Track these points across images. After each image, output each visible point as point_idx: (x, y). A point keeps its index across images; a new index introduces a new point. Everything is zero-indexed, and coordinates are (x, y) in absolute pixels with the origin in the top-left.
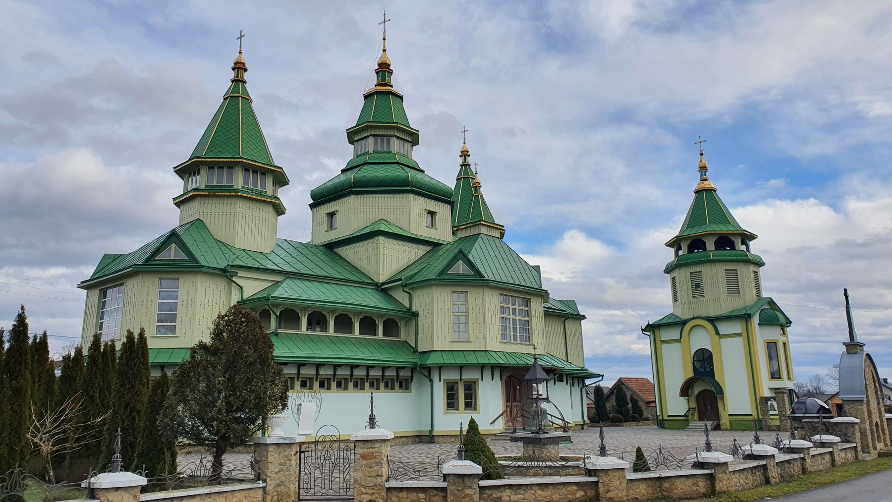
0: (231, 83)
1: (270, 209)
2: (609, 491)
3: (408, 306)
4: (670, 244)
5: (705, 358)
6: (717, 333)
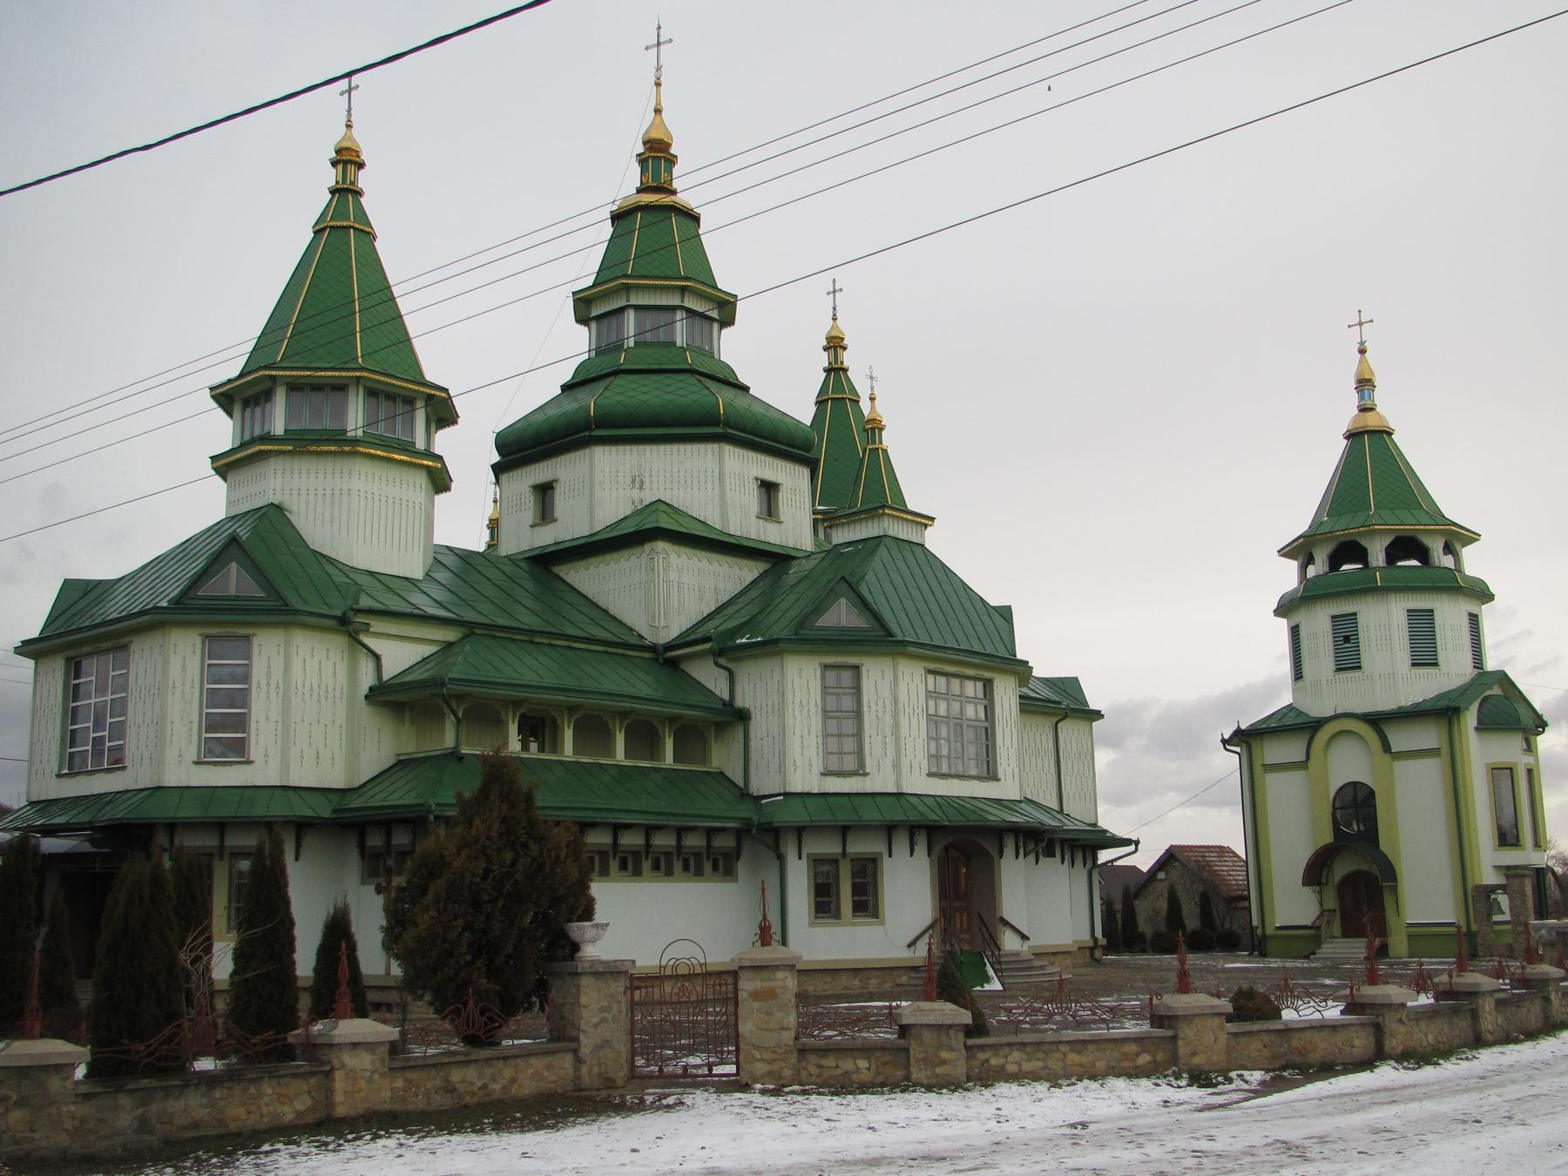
0: (330, 196)
1: (422, 480)
3: (726, 696)
4: (1288, 552)
5: (1359, 800)
6: (1386, 747)
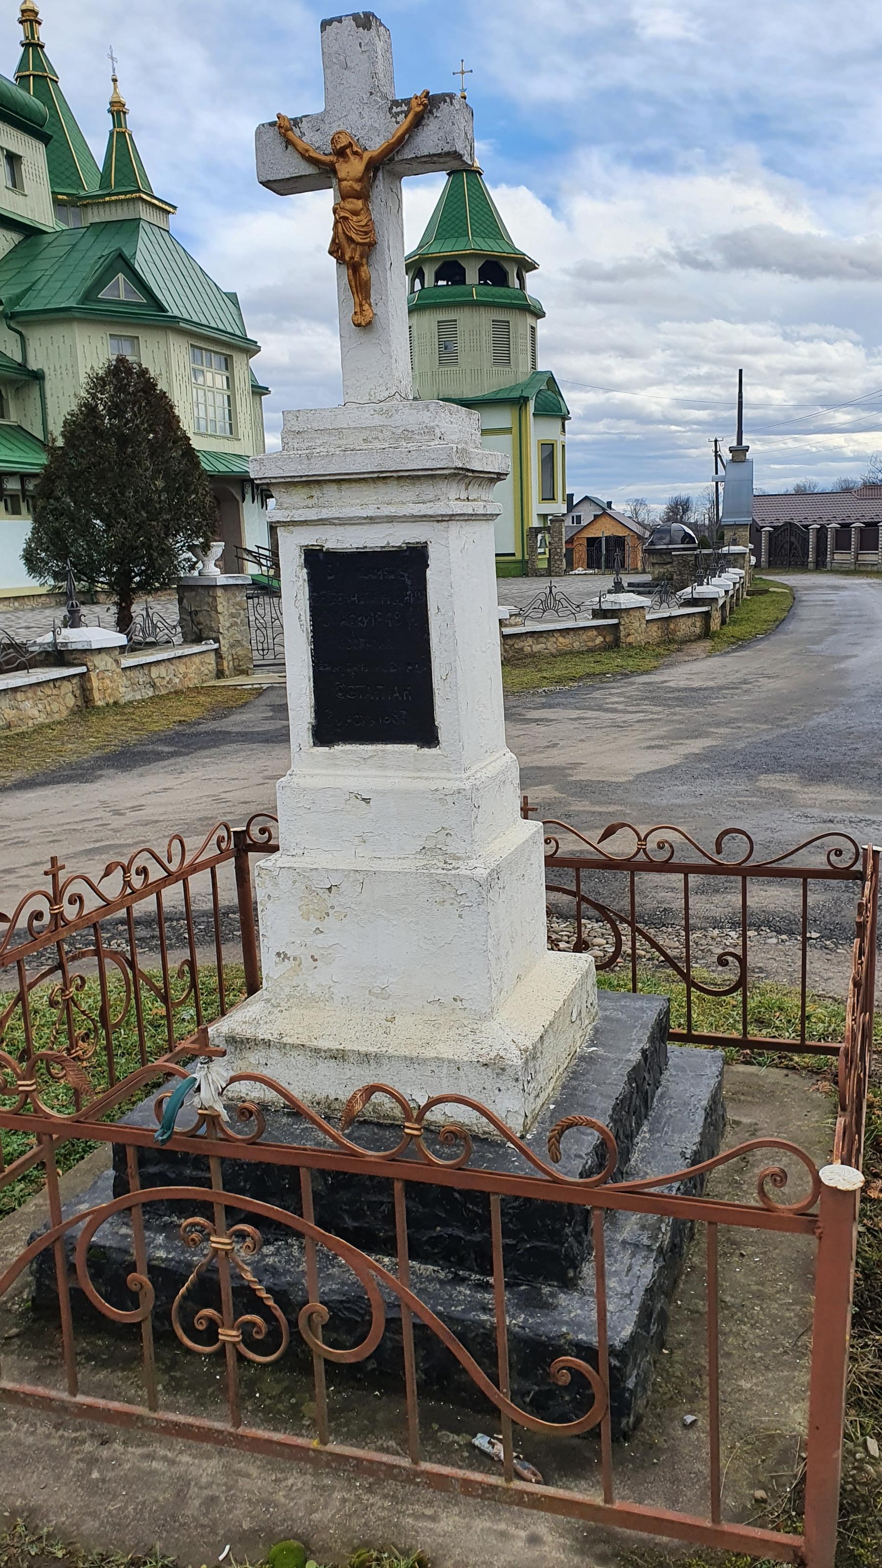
2: (629, 635)
3: (20, 360)
